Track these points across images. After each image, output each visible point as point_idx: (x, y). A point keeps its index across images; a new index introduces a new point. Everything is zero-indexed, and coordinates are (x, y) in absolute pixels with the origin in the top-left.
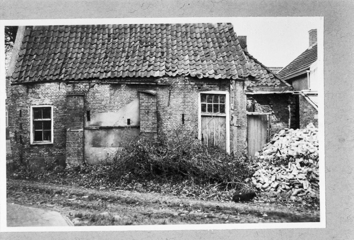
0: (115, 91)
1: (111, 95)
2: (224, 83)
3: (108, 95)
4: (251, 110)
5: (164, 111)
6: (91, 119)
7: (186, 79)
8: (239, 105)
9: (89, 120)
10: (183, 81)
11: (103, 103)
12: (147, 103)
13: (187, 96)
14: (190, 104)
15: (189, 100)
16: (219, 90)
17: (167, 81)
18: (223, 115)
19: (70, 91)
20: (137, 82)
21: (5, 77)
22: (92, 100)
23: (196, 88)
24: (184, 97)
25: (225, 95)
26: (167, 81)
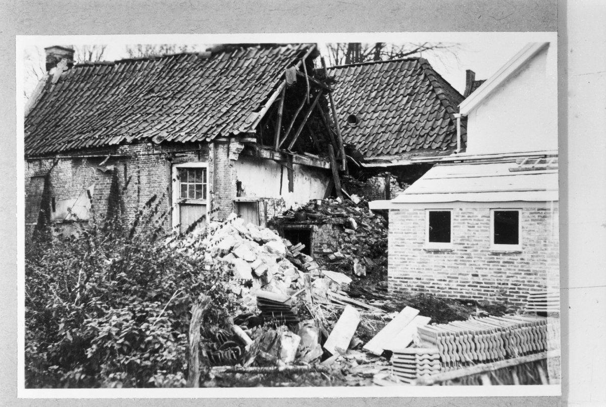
0: (76, 169)
1: (74, 174)
2: (199, 148)
3: (71, 175)
4: (383, 196)
5: (128, 197)
6: (56, 210)
7: (149, 146)
8: (223, 185)
9: (54, 210)
10: (146, 149)
11: (67, 186)
12: (101, 184)
13: (152, 173)
14: (156, 185)
15: (155, 178)
16: (197, 160)
17: (128, 150)
18: (200, 201)
19: (37, 170)
20: (90, 154)
21: (330, 42)
22: (56, 182)
23: (163, 158)
24: (149, 175)
25: (204, 169)
26: (128, 150)
